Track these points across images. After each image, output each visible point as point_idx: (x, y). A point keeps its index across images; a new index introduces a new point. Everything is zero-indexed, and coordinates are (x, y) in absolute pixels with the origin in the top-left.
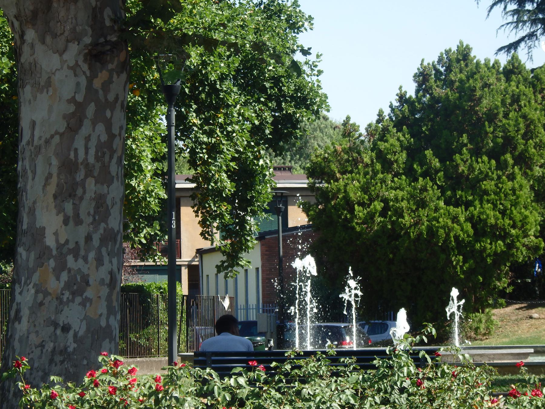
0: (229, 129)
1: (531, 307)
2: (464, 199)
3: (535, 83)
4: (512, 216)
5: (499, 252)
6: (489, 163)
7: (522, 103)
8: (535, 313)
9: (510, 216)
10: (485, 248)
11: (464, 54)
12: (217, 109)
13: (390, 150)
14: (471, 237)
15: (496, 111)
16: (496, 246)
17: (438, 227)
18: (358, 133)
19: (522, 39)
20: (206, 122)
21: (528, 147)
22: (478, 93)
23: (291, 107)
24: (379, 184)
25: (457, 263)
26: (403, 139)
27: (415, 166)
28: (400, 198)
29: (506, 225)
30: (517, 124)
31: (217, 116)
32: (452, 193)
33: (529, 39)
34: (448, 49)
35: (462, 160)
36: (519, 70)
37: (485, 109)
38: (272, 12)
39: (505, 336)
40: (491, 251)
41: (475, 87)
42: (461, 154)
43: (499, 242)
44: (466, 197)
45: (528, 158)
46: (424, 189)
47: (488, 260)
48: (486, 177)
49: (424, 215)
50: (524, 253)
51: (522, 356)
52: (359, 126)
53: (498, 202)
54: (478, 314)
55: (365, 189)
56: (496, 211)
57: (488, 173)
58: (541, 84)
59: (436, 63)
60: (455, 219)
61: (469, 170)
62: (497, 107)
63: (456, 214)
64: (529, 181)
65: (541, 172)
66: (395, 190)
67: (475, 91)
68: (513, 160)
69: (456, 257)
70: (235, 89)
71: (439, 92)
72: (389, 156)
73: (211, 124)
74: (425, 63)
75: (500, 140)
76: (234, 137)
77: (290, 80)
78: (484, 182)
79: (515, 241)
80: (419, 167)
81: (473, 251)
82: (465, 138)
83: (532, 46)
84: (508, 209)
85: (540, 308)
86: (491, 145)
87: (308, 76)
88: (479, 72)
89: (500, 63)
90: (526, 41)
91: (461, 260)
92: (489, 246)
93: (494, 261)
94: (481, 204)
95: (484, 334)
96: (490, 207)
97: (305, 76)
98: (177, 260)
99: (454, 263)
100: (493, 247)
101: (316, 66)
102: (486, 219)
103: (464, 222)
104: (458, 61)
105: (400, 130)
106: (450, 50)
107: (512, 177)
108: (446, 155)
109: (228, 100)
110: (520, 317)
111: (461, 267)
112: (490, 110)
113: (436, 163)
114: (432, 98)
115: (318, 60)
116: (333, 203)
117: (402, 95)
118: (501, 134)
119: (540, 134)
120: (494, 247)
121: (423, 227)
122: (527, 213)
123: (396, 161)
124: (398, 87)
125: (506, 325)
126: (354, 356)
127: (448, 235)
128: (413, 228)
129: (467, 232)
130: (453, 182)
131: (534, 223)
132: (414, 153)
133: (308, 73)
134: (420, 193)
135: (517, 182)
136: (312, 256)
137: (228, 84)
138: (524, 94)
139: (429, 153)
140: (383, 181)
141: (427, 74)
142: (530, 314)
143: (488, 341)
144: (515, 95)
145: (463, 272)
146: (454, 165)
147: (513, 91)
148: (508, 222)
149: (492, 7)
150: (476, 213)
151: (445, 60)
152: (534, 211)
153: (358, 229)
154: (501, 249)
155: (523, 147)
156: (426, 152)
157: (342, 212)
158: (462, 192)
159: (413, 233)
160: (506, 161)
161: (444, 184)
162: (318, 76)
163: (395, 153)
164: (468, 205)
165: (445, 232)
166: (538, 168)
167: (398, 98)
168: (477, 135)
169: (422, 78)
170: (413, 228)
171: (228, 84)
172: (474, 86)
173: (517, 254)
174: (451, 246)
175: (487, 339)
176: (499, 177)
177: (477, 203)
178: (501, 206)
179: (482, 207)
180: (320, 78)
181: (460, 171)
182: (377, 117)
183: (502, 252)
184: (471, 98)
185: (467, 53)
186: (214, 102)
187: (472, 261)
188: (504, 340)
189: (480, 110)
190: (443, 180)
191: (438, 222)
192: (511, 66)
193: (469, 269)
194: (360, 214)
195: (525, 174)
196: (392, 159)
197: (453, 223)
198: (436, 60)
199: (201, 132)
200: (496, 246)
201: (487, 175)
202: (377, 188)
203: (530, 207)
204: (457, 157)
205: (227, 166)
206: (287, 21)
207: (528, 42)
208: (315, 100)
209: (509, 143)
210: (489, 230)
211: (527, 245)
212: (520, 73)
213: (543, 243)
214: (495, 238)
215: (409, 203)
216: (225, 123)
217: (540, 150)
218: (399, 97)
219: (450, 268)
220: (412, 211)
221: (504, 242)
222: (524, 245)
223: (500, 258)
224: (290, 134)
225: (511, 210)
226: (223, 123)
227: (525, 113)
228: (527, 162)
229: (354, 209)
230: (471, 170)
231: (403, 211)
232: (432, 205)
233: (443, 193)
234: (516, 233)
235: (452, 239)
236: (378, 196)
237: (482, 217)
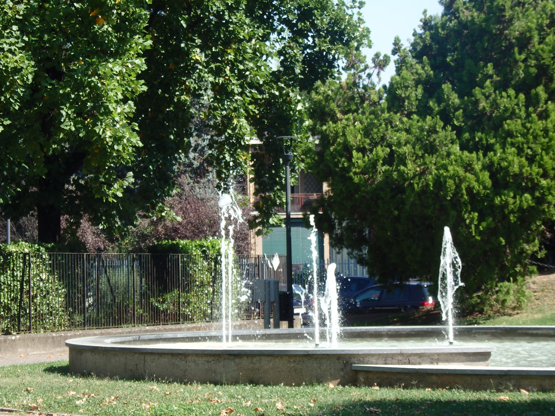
0: (241, 67)
2: (484, 142)
4: (542, 162)
5: (525, 207)
6: (516, 97)
10: (507, 204)
12: (227, 44)
13: (400, 84)
14: (488, 189)
15: (528, 34)
16: (521, 201)
17: (445, 177)
18: (363, 64)
20: (214, 58)
22: (508, 14)
23: (326, 42)
25: (471, 222)
26: (422, 72)
27: (431, 103)
28: (403, 141)
29: (534, 174)
31: (226, 52)
32: (470, 135)
35: (484, 94)
39: (540, 311)
40: (515, 207)
41: (504, 6)
42: (482, 87)
43: (526, 195)
44: (487, 140)
46: (433, 130)
47: (511, 218)
48: (513, 115)
49: (431, 163)
51: (480, 357)
52: (365, 57)
53: (525, 146)
54: (506, 283)
55: (367, 132)
57: (514, 110)
60: (468, 167)
61: (492, 106)
62: (530, 30)
63: (469, 161)
67: (504, 10)
68: (546, 92)
69: (470, 214)
70: (247, 21)
72: (399, 92)
73: (218, 61)
75: (533, 70)
76: (247, 75)
77: (325, 12)
78: (508, 121)
79: (546, 194)
80: (436, 105)
81: (492, 206)
82: (490, 69)
84: (538, 155)
87: (348, 8)
91: (476, 218)
93: (519, 218)
95: (514, 309)
96: (514, 152)
97: (345, 8)
98: (291, 213)
99: (468, 221)
102: (507, 167)
103: (481, 170)
105: (421, 62)
108: (464, 91)
109: (239, 33)
111: (477, 227)
112: (521, 34)
113: (455, 99)
114: (460, 22)
116: (332, 149)
117: (426, 21)
118: (533, 62)
121: (430, 176)
123: (408, 98)
124: (422, 11)
125: (546, 296)
127: (458, 186)
128: (417, 178)
130: (475, 121)
132: (431, 88)
133: (348, 5)
134: (429, 136)
137: (240, 15)
139: (446, 87)
140: (389, 122)
143: (519, 316)
145: (480, 233)
146: (472, 100)
148: (537, 170)
150: (495, 159)
153: (356, 179)
154: (528, 204)
156: (444, 86)
157: (338, 160)
158: (482, 134)
159: (418, 184)
160: (537, 95)
161: (463, 124)
162: (360, 8)
163: (407, 87)
164: (489, 148)
165: (455, 183)
167: (421, 24)
168: (504, 64)
170: (417, 178)
171: (240, 15)
173: (549, 211)
174: (462, 200)
175: (518, 313)
176: (528, 115)
177: (497, 146)
179: (504, 152)
180: (361, 11)
182: (392, 47)
183: (530, 208)
184: (500, 19)
186: (222, 36)
187: (491, 219)
188: (536, 316)
189: (510, 34)
190: (461, 120)
191: (447, 171)
193: (488, 228)
194: (360, 161)
196: (403, 95)
199: (206, 70)
200: (521, 201)
201: (513, 113)
202: (381, 130)
204: (477, 91)
205: (246, 110)
208: (354, 34)
210: (511, 180)
214: (520, 190)
215: (414, 148)
216: (236, 60)
219: (462, 227)
220: (418, 157)
221: (532, 195)
223: (527, 216)
224: (326, 73)
225: (542, 157)
226: (233, 60)
229: (351, 156)
230: (495, 106)
231: (406, 158)
232: (443, 151)
233: (459, 135)
234: (548, 184)
235: (464, 192)
236: (383, 138)
237: (502, 164)
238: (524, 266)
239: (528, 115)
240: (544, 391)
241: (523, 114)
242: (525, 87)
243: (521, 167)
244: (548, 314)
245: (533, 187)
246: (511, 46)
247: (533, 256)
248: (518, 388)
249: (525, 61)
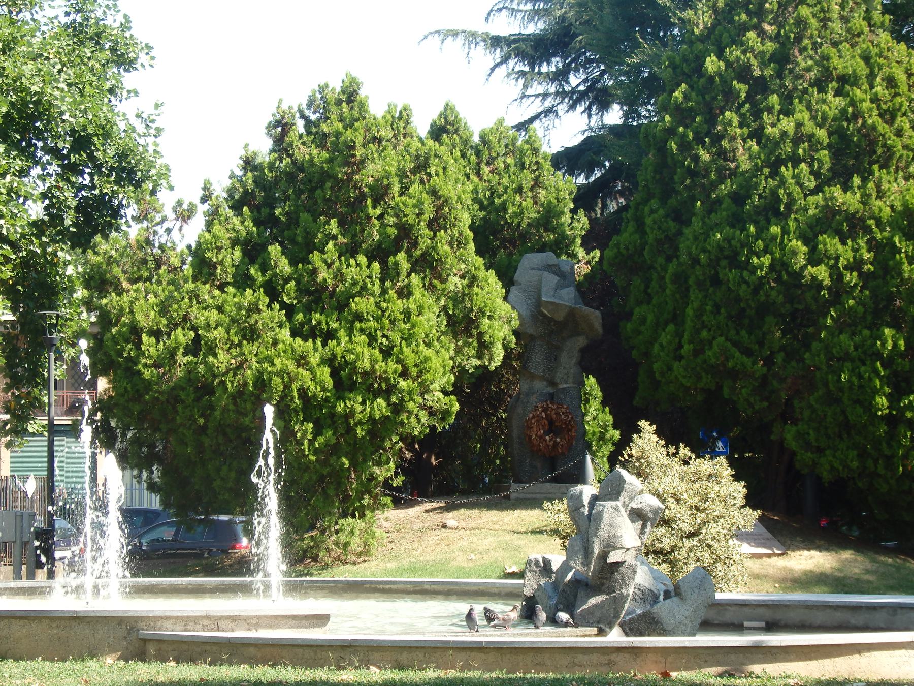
1: (449, 508)
2: (324, 326)
3: (481, 148)
4: (400, 356)
5: (377, 417)
6: (368, 267)
7: (433, 170)
8: (451, 518)
9: (397, 357)
10: (352, 413)
11: (350, 95)
13: (211, 244)
14: (328, 391)
15: (386, 182)
16: (372, 409)
17: (270, 373)
18: (160, 215)
21: (437, 243)
22: (359, 152)
23: (109, 183)
24: (187, 300)
26: (241, 228)
33: (545, 117)
34: (322, 84)
35: (325, 261)
37: (371, 179)
38: (83, 34)
40: (364, 416)
42: (322, 252)
44: (327, 324)
45: (436, 261)
46: (254, 309)
47: (358, 432)
49: (250, 353)
50: (423, 420)
52: (163, 205)
55: (163, 309)
56: (374, 348)
57: (365, 283)
58: (489, 149)
59: (304, 106)
60: (301, 360)
61: (335, 277)
62: (388, 176)
63: (303, 352)
64: (438, 299)
65: (460, 286)
66: (211, 310)
69: (303, 424)
71: (302, 152)
74: (285, 107)
75: (392, 231)
80: (260, 273)
81: (333, 415)
85: (462, 511)
86: (377, 238)
87: (139, 135)
88: (364, 118)
89: (411, 110)
91: (310, 431)
92: (359, 408)
93: (369, 432)
95: (360, 555)
99: (299, 435)
100: (358, 407)
101: (153, 121)
103: (319, 365)
104: (339, 102)
106: (327, 86)
107: (405, 293)
111: (311, 442)
112: (377, 181)
113: (284, 266)
115: (157, 112)
120: (368, 410)
123: (221, 263)
124: (243, 145)
125: (402, 538)
127: (287, 387)
128: (231, 374)
129: (321, 383)
130: (312, 298)
131: (442, 370)
132: (253, 251)
138: (436, 156)
141: (287, 124)
142: (444, 521)
145: (316, 452)
148: (394, 367)
149: (493, 70)
150: (339, 350)
151: (318, 101)
152: (442, 350)
153: (147, 374)
155: (429, 241)
157: (122, 346)
159: (232, 382)
160: (396, 264)
161: (295, 302)
163: (219, 249)
164: (330, 335)
165: (283, 382)
166: (457, 279)
169: (280, 129)
170: (231, 374)
173: (409, 422)
174: (293, 406)
175: (364, 561)
176: (384, 292)
177: (342, 333)
178: (384, 340)
179: (351, 340)
180: (158, 140)
181: (320, 279)
185: (355, 91)
187: (330, 432)
188: (389, 565)
191: (273, 364)
192: (443, 121)
194: (152, 350)
195: (430, 288)
196: (215, 260)
197: (298, 366)
198: (304, 102)
200: (372, 409)
201: (364, 288)
202: (183, 307)
203: (436, 343)
204: (315, 256)
206: (113, 50)
207: (544, 120)
209: (405, 233)
210: (359, 380)
211: (431, 407)
212: (456, 132)
214: (372, 393)
215: (228, 332)
218: (245, 162)
221: (387, 400)
222: (422, 407)
223: (379, 429)
227: (434, 187)
229: (140, 341)
230: (339, 278)
232: (268, 337)
234: (409, 386)
236: (185, 318)
237: (348, 358)
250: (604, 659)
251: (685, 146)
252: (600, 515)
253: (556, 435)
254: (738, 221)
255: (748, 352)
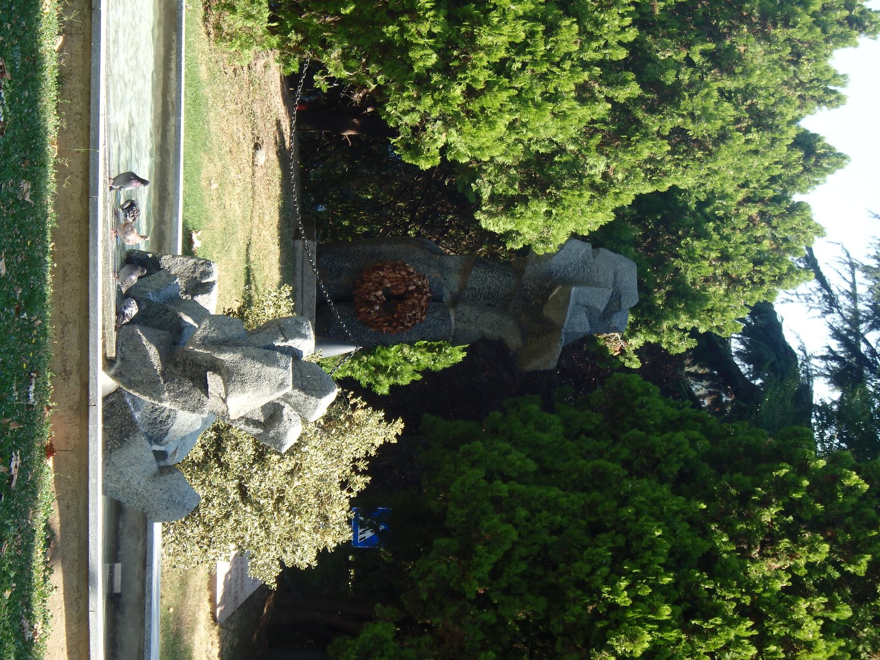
4: (496, 88)
5: (411, 54)
6: (620, 43)
7: (754, 136)
8: (268, 157)
15: (738, 70)
16: (423, 47)
19: (820, 277)
21: (653, 140)
22: (779, 33)
29: (474, 73)
30: (709, 118)
33: (824, 296)
36: (813, 168)
41: (793, 27)
45: (629, 139)
50: (406, 119)
57: (597, 38)
58: (782, 216)
62: (747, 73)
64: (575, 141)
67: (786, 25)
75: (670, 78)
83: (811, 303)
86: (661, 56)
88: (827, 41)
89: (837, 106)
90: (820, 290)
92: (424, 28)
93: (390, 42)
94: (526, 17)
95: (218, 27)
107: (584, 95)
110: (260, 123)
112: (740, 57)
119: (683, 174)
120: (421, 41)
122: (501, 126)
125: (241, 88)
126: (354, 535)
131: (476, 145)
135: (573, 108)
136: (387, 480)
138: (774, 140)
142: (264, 146)
144: (774, 119)
147: (781, 114)
148: (481, 78)
152: (504, 146)
155: (655, 129)
160: (624, 83)
172: (796, 23)
173: (404, 99)
175: (209, 34)
176: (586, 65)
178: (519, 65)
179: (518, 18)
183: (409, 65)
185: (865, 28)
188: (203, 68)
189: (741, 36)
192: (822, 151)
195: (591, 129)
200: (423, 47)
201: (591, 37)
207: (820, 294)
209: (665, 97)
210: (463, 30)
211: (424, 130)
212: (807, 170)
213: (428, 167)
217: (646, 171)
221: (434, 69)
223: (394, 56)
227: (731, 138)
228: (619, 139)
234: (454, 99)
237: (494, 13)
238: (298, 49)
239: (586, 65)
240: (61, 80)
241: (589, 55)
242: (639, 60)
243: (489, 49)
244: (207, 91)
245: (448, 70)
246: (717, 37)
247: (317, 67)
248: (66, 31)
249: (689, 62)
250: (72, 365)
251: (783, 487)
252: (274, 362)
253: (383, 305)
254: (678, 560)
255: (496, 573)
